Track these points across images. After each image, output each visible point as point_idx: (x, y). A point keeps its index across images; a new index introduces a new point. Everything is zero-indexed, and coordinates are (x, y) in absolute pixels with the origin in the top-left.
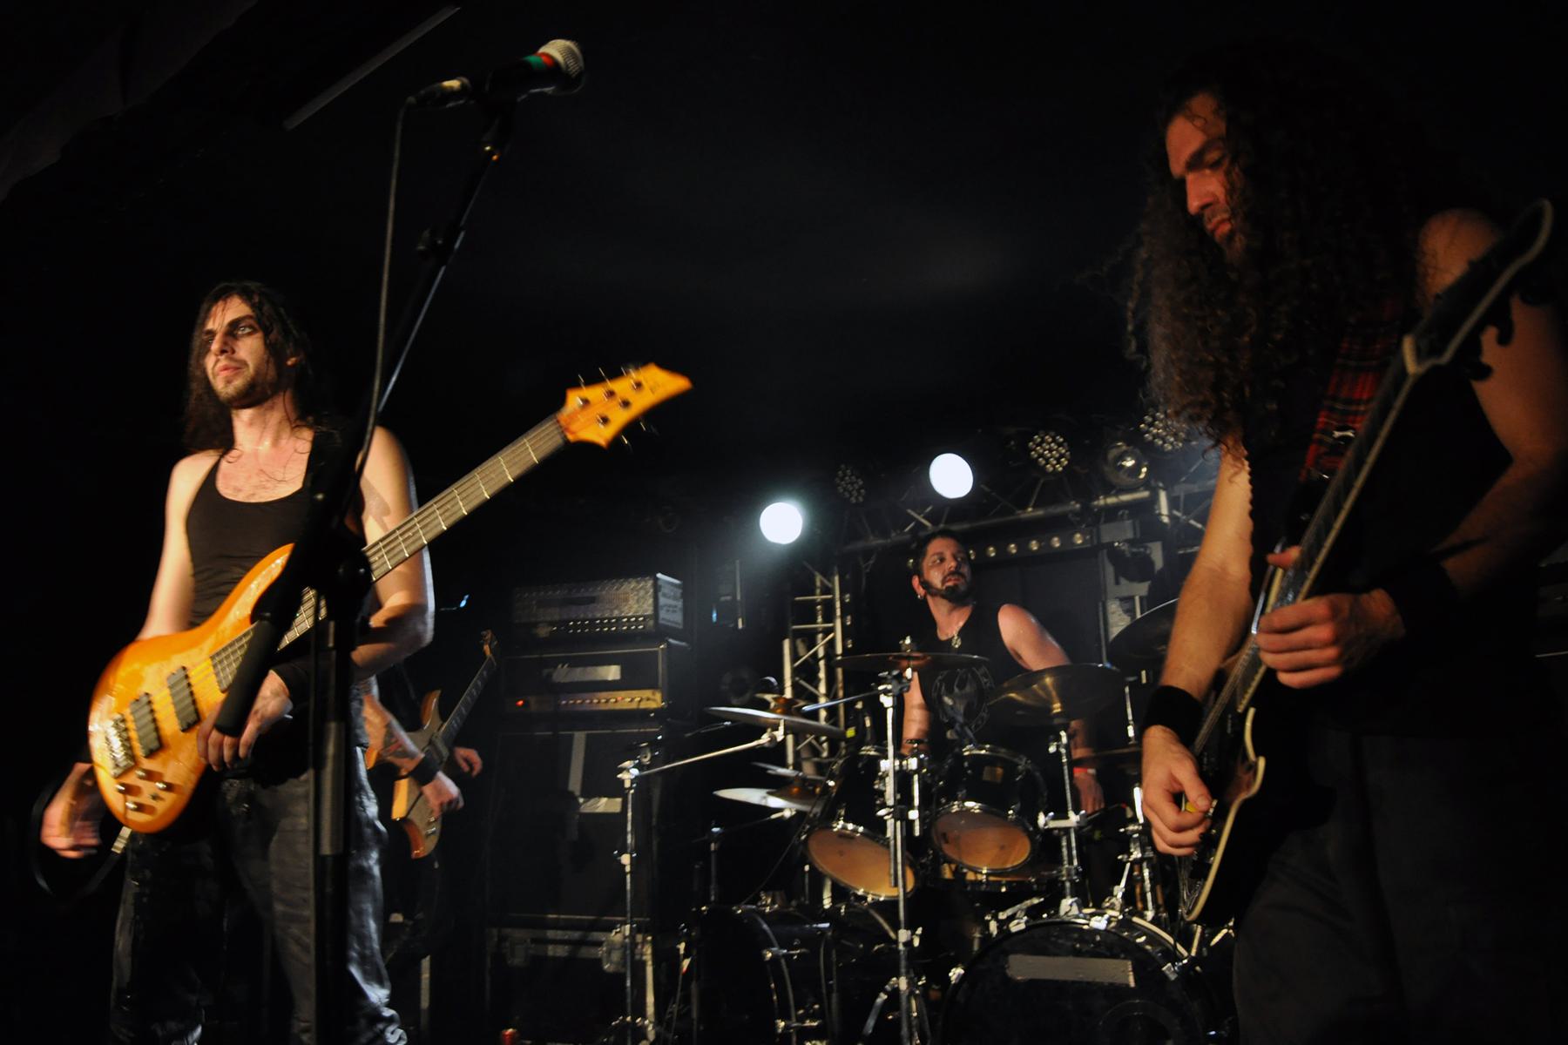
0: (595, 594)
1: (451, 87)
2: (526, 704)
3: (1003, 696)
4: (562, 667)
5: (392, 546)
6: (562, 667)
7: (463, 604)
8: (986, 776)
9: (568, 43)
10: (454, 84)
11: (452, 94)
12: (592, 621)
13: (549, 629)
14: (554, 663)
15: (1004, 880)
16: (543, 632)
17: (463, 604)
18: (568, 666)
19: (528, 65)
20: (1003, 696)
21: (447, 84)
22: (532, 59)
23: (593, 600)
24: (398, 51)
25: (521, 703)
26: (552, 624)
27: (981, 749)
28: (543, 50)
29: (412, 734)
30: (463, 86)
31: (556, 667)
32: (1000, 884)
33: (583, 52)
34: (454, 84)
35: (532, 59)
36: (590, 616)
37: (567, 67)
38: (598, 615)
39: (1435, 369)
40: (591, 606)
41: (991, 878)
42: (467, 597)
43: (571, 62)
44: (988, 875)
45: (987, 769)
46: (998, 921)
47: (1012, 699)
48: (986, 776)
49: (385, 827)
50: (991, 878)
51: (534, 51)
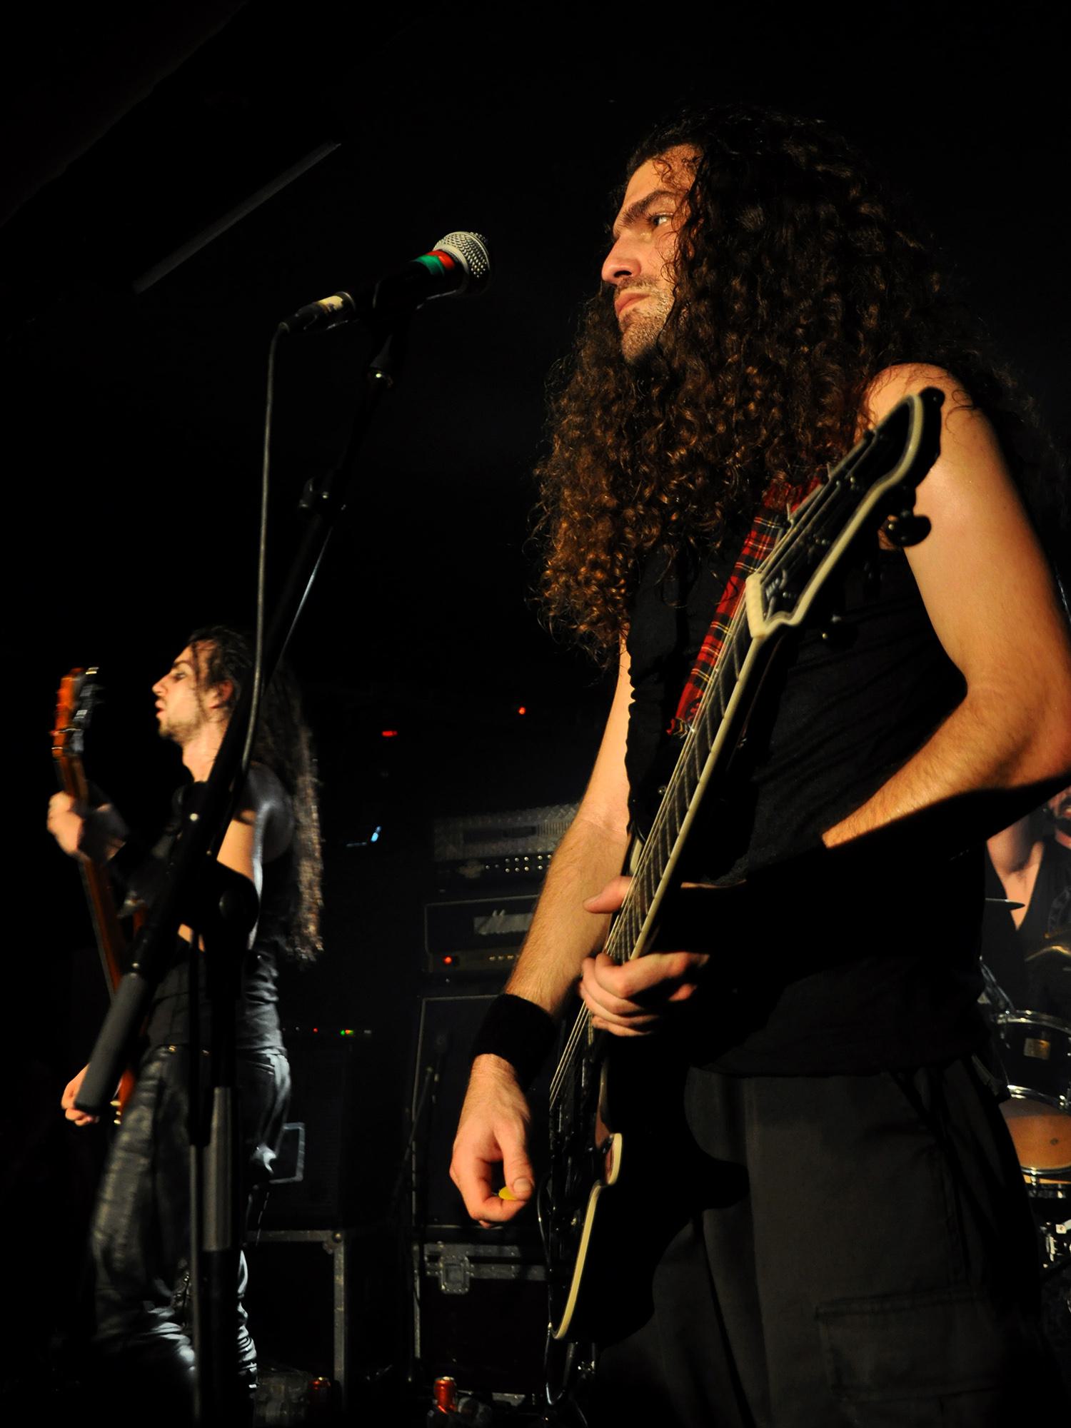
0: (535, 824)
1: (332, 306)
2: (455, 960)
3: (1045, 950)
4: (498, 914)
5: (584, 1014)
6: (498, 914)
7: (375, 837)
8: (1028, 1051)
9: (471, 236)
10: (334, 301)
11: (333, 313)
12: (533, 856)
13: (482, 867)
14: (486, 911)
15: (1060, 1183)
16: (472, 871)
17: (375, 837)
18: (505, 914)
19: (423, 267)
20: (1045, 950)
21: (326, 302)
22: (428, 259)
23: (533, 831)
24: (309, 167)
25: (448, 960)
26: (483, 861)
27: (1019, 1017)
28: (440, 246)
29: (250, 878)
30: (345, 302)
31: (490, 914)
32: (1055, 1189)
33: (487, 246)
34: (334, 301)
35: (428, 259)
36: (530, 850)
37: (470, 265)
38: (539, 850)
39: (782, 629)
40: (531, 839)
41: (1043, 1181)
42: (378, 829)
43: (475, 261)
44: (1037, 1176)
45: (1028, 1041)
46: (1056, 1236)
47: (1057, 953)
48: (1028, 1051)
49: (272, 1167)
50: (1043, 1181)
51: (428, 249)
